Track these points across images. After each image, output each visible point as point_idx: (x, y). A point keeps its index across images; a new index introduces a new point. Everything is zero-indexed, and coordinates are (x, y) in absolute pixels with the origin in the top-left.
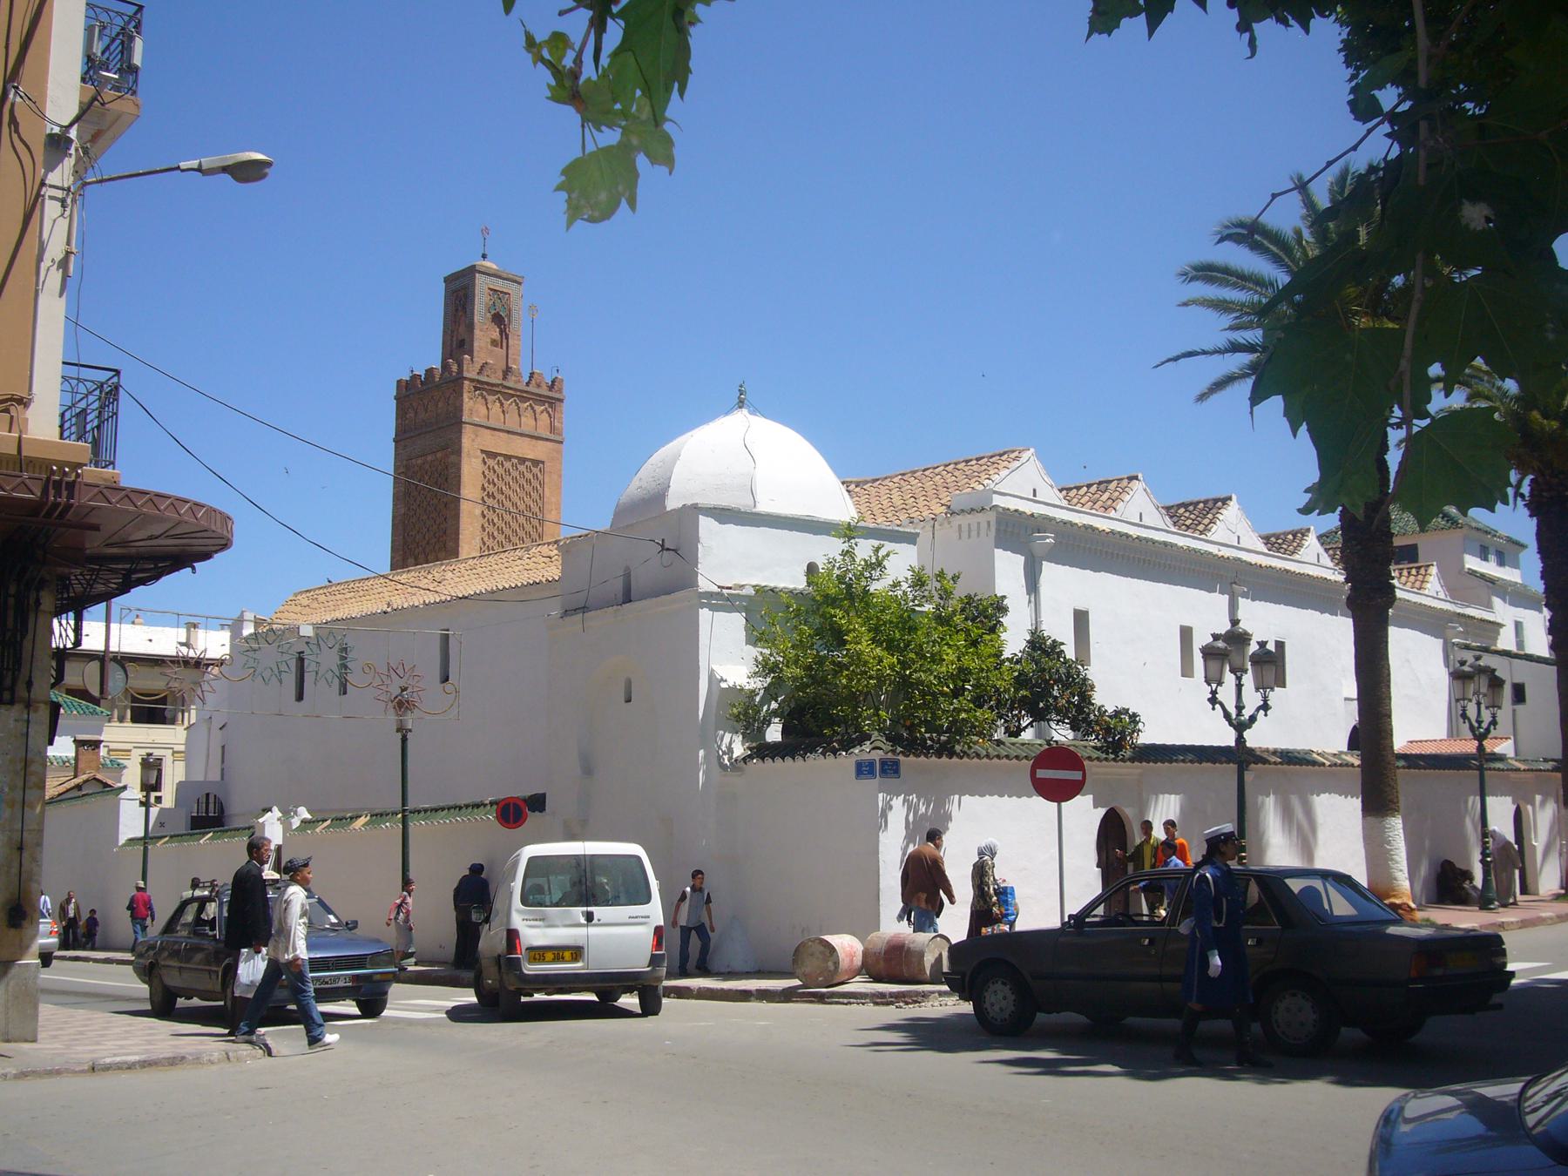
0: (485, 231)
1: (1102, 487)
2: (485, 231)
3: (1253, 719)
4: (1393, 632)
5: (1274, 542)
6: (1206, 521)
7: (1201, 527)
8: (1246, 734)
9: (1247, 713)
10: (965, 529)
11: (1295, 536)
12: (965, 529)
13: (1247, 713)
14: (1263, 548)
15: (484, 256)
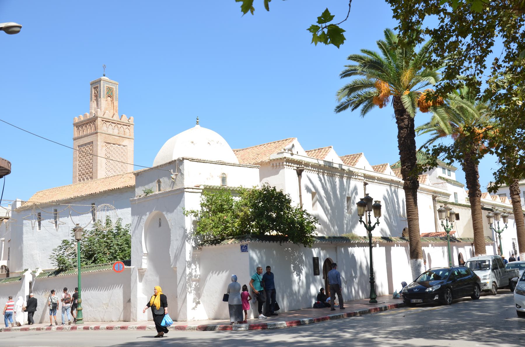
0: (104, 67)
1: (320, 151)
2: (104, 67)
3: (374, 227)
4: (418, 193)
5: (376, 169)
6: (354, 162)
7: (352, 164)
8: (372, 232)
9: (372, 225)
10: (275, 165)
11: (383, 166)
12: (275, 165)
13: (372, 225)
14: (373, 170)
15: (104, 76)
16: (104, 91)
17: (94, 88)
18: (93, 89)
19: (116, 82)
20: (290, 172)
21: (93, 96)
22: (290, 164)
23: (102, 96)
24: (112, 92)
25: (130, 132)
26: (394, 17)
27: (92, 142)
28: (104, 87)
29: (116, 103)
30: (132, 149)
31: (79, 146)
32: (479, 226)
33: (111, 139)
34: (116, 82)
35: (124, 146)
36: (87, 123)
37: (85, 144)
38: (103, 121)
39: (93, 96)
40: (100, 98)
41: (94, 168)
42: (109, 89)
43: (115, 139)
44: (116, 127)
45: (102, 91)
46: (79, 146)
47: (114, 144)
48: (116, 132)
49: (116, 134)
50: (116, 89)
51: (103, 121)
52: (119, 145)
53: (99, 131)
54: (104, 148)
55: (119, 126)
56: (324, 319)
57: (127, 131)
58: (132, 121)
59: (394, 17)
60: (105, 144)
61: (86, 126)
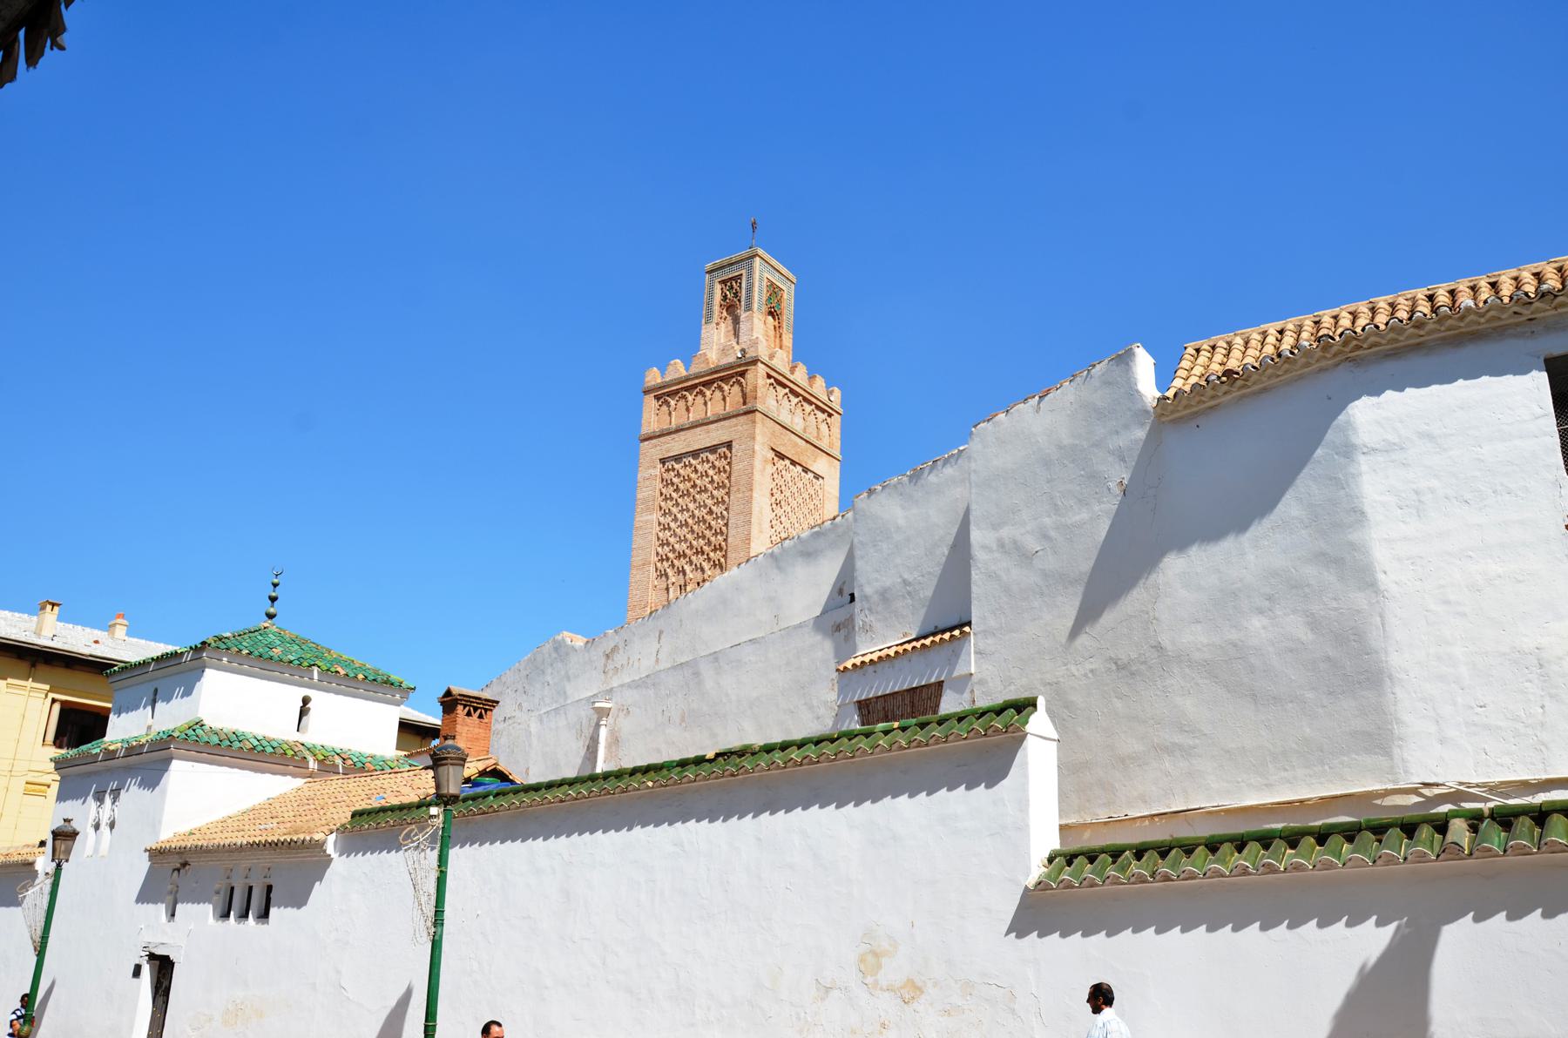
16: (760, 291)
17: (723, 282)
18: (718, 287)
19: (791, 276)
20: (903, 743)
21: (716, 308)
22: (900, 649)
23: (755, 306)
24: (779, 302)
25: (830, 434)
26: (448, 693)
27: (729, 445)
28: (761, 279)
29: (788, 339)
30: (836, 483)
31: (663, 461)
32: (42, 669)
33: (789, 445)
34: (791, 276)
35: (817, 477)
36: (707, 384)
37: (695, 454)
38: (769, 376)
39: (716, 308)
40: (749, 308)
41: (732, 532)
42: (774, 290)
43: (796, 445)
44: (799, 410)
45: (756, 289)
46: (663, 461)
47: (793, 463)
48: (797, 423)
49: (798, 428)
50: (788, 294)
51: (769, 376)
52: (806, 470)
53: (759, 407)
54: (770, 469)
55: (808, 408)
56: (504, 794)
57: (824, 427)
58: (837, 396)
59: (448, 693)
60: (772, 454)
61: (702, 393)
